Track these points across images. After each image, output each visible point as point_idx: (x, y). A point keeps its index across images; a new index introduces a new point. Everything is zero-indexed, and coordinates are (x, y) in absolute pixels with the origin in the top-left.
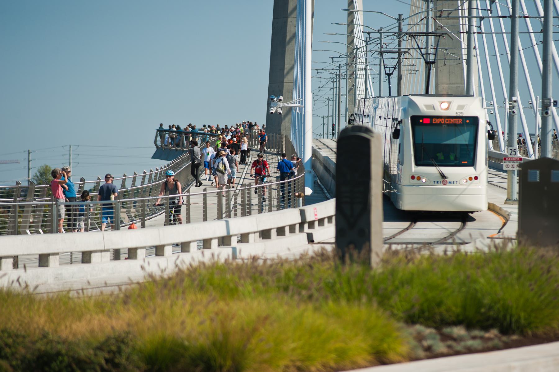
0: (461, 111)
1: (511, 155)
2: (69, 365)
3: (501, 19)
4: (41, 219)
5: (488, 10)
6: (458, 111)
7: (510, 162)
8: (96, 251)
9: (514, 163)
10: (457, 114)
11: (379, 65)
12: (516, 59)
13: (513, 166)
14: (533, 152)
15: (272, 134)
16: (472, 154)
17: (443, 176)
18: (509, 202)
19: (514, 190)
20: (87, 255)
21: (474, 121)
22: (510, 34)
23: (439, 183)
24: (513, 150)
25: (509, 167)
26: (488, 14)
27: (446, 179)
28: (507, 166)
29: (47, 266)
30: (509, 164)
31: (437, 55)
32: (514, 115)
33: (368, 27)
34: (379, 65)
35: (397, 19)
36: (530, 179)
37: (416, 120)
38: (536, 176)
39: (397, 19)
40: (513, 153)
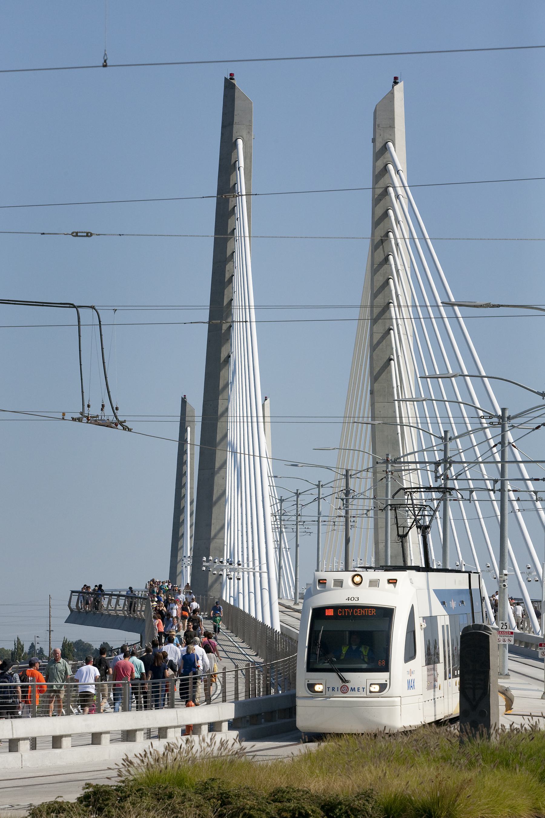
1: (502, 629)
2: (346, 812)
4: (29, 694)
5: (489, 490)
8: (171, 727)
11: (317, 521)
12: (506, 533)
13: (504, 640)
14: (539, 628)
15: (202, 596)
18: (501, 676)
19: (505, 664)
20: (163, 730)
23: (336, 689)
26: (469, 484)
29: (135, 741)
30: (500, 637)
32: (504, 589)
33: (308, 481)
34: (317, 521)
35: (344, 475)
39: (344, 475)
40: (504, 627)
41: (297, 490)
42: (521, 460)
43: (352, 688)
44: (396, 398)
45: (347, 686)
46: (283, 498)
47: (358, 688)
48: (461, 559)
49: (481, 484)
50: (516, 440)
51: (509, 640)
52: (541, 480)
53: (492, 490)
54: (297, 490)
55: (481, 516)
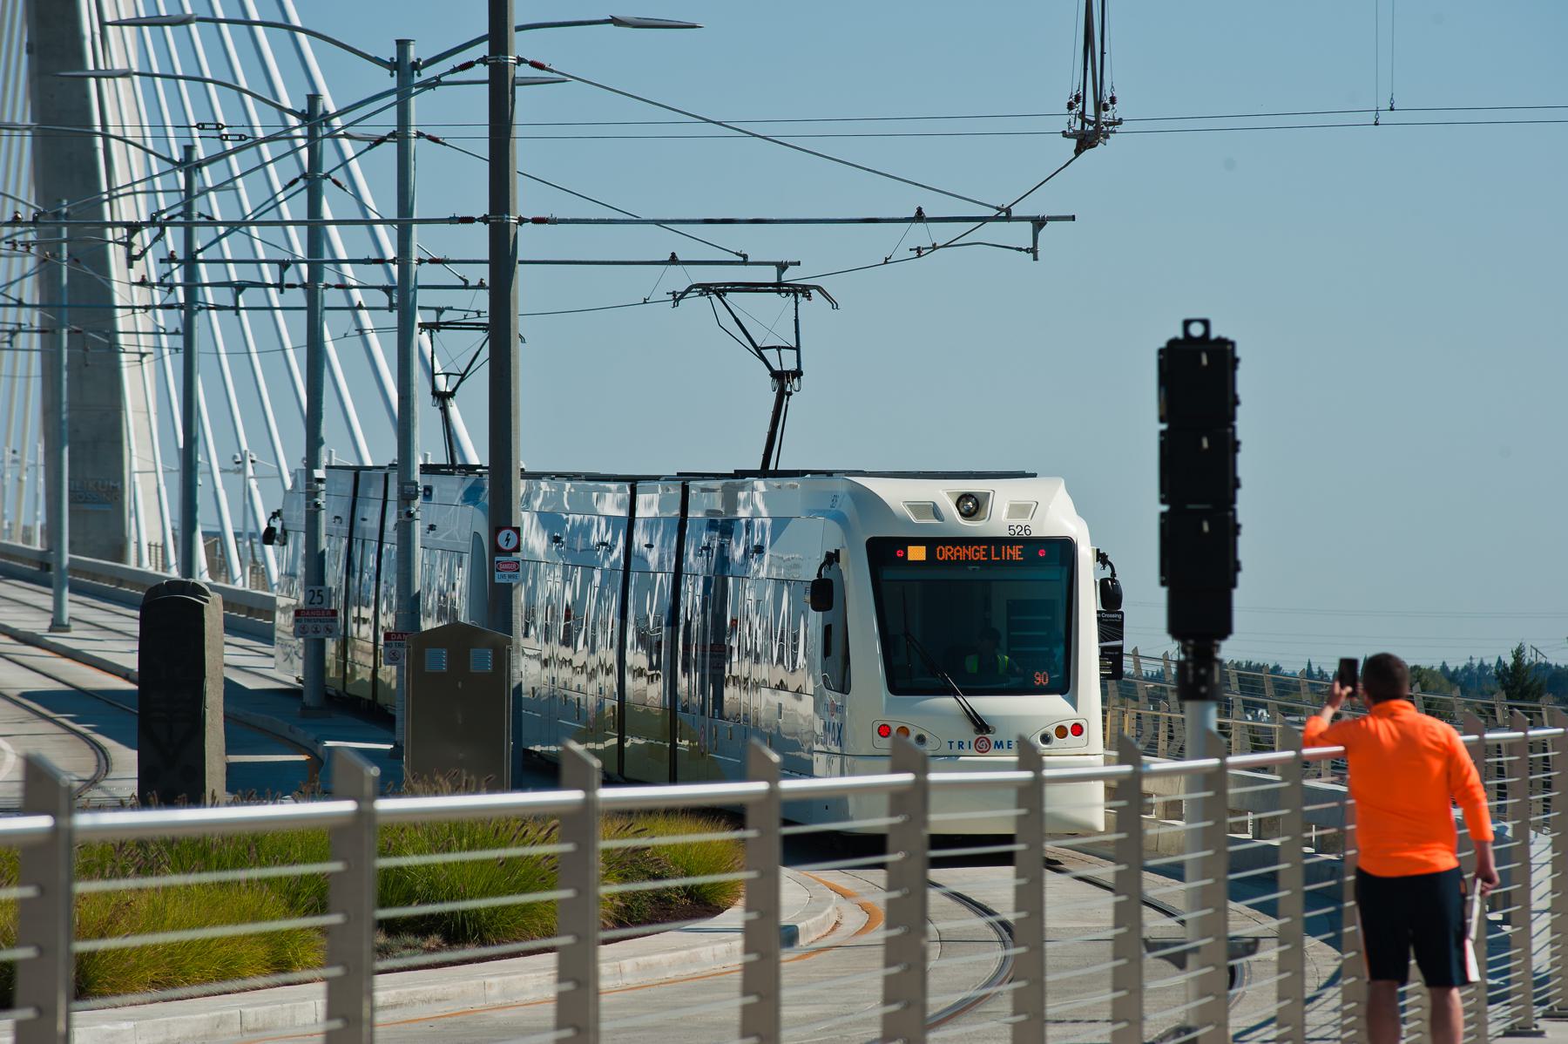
0: (1023, 522)
3: (213, 313)
6: (1015, 522)
7: (309, 621)
9: (318, 623)
10: (1012, 532)
13: (316, 628)
16: (1060, 651)
17: (980, 725)
21: (1064, 549)
22: (395, 335)
23: (966, 746)
24: (316, 592)
25: (307, 632)
27: (987, 735)
28: (301, 630)
31: (431, 374)
36: (429, 667)
37: (884, 552)
38: (438, 661)
41: (402, 45)
42: (331, 218)
43: (996, 742)
44: (91, 66)
45: (987, 739)
46: (413, 54)
47: (1009, 742)
48: (244, 446)
49: (250, 273)
50: (361, 153)
51: (327, 629)
52: (479, 220)
53: (275, 286)
54: (402, 45)
55: (253, 349)
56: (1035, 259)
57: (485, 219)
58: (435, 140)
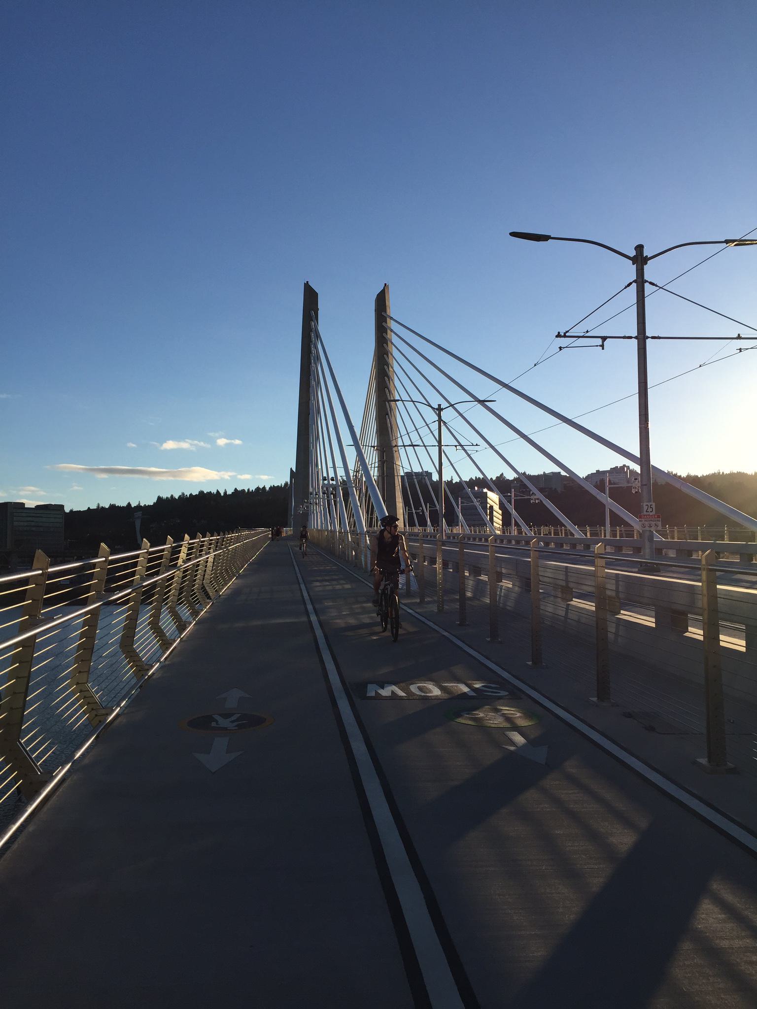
9: (651, 522)
51: (656, 525)
52: (634, 338)
56: (603, 349)
57: (636, 338)
58: (741, 243)
